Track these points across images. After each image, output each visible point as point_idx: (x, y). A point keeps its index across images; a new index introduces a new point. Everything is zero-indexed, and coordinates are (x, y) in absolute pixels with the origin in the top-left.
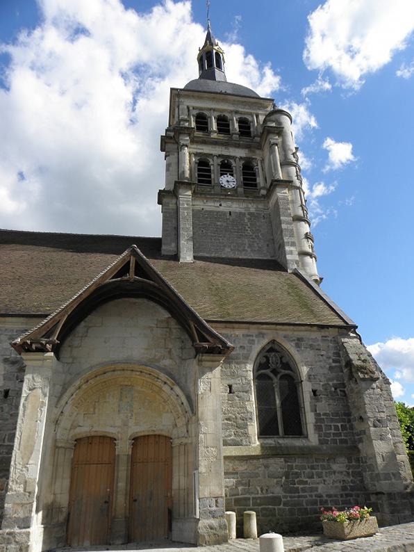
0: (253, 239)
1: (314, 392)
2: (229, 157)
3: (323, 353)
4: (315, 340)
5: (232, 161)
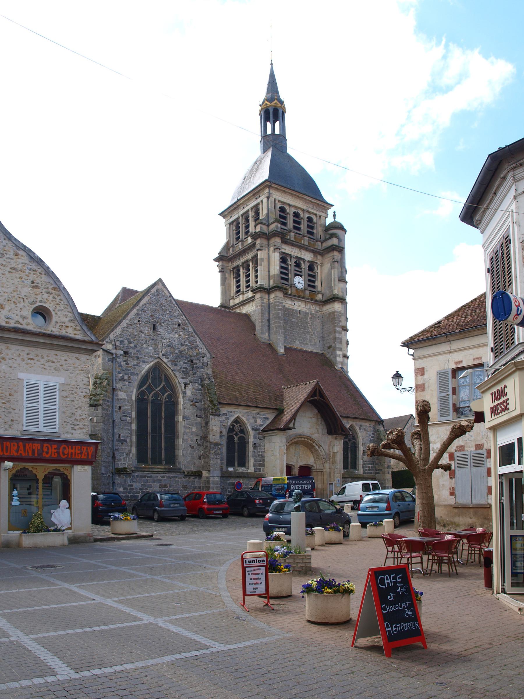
0: (312, 335)
1: (363, 450)
2: (301, 259)
3: (369, 433)
4: (366, 426)
5: (302, 262)
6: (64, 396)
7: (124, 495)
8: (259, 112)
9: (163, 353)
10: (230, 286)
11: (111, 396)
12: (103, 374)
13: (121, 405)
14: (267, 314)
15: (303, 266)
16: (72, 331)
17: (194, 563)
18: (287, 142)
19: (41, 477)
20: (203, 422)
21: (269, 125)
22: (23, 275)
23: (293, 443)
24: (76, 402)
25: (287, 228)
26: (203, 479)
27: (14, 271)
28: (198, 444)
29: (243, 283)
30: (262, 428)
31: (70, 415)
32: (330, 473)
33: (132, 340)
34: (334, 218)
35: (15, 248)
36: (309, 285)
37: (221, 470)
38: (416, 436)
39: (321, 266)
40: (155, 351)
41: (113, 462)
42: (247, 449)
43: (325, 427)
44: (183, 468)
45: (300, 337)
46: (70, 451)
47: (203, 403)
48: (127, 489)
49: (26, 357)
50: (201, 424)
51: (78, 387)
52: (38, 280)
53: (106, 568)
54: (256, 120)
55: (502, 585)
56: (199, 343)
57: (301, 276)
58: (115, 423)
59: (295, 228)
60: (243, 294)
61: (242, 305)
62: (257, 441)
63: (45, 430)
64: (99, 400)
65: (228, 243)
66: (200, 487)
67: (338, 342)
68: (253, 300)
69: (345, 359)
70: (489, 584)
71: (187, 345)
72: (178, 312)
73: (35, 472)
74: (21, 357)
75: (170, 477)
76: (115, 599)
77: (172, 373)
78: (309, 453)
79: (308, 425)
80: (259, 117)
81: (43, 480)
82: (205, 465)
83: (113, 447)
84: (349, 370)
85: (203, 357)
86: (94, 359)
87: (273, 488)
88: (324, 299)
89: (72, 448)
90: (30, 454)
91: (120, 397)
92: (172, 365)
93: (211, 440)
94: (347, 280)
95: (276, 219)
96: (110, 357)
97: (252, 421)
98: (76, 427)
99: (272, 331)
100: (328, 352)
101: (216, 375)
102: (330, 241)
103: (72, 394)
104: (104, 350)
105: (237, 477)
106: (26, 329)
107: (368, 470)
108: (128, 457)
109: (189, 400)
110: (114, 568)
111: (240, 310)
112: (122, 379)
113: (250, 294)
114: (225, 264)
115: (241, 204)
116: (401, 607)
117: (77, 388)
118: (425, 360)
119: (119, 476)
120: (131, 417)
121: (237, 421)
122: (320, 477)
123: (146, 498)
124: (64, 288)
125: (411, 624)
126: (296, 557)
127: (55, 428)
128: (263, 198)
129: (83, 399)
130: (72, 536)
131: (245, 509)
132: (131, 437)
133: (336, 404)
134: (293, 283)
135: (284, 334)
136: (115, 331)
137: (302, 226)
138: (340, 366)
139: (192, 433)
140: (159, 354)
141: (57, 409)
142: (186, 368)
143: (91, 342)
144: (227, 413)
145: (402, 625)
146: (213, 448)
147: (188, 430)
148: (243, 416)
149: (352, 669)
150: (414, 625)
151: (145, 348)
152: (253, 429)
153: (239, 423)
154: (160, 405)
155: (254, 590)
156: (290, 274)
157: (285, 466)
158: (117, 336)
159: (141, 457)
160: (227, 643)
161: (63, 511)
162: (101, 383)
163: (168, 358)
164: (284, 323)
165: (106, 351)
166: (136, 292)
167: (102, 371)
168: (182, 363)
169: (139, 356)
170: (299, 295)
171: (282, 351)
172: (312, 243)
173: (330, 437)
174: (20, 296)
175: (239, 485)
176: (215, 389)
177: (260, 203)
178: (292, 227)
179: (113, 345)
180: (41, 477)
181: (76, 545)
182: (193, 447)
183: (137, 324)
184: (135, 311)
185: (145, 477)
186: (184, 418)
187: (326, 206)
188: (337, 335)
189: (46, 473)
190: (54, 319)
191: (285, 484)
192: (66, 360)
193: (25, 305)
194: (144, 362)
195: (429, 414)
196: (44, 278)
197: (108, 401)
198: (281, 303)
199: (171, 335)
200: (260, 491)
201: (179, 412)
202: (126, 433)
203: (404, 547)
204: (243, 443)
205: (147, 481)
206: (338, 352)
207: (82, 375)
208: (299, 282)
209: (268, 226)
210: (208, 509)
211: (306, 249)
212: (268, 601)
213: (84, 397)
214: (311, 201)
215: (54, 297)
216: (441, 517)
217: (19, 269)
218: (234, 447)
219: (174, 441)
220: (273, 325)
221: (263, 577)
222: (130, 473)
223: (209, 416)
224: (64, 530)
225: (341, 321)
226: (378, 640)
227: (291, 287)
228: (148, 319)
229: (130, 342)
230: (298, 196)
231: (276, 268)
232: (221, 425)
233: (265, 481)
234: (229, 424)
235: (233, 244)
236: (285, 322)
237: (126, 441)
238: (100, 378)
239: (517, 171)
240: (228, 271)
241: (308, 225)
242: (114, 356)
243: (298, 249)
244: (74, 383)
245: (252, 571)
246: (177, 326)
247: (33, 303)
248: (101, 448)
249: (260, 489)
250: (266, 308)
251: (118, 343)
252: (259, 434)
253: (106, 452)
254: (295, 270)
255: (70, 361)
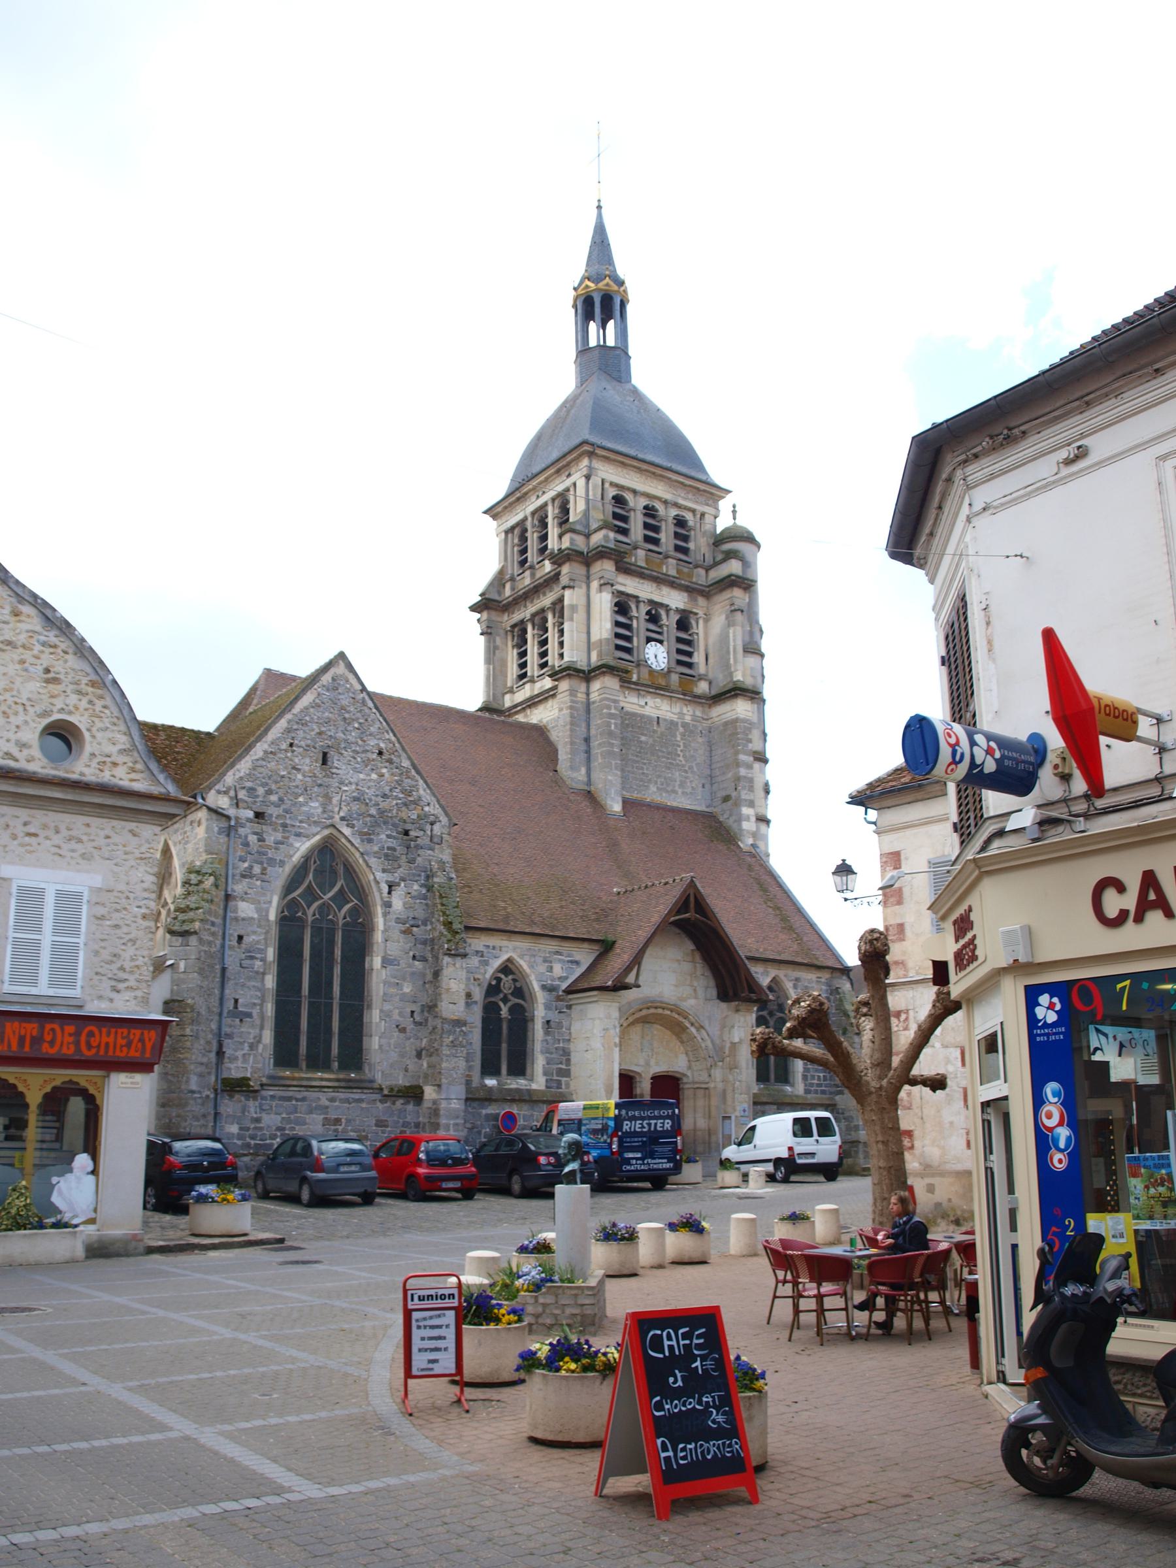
2: (661, 605)
4: (810, 981)
6: (99, 915)
7: (239, 1142)
8: (571, 302)
9: (342, 814)
10: (504, 663)
11: (221, 912)
12: (205, 863)
13: (241, 932)
14: (584, 725)
15: (664, 620)
16: (130, 773)
17: (345, 1305)
18: (632, 361)
19: (34, 1098)
20: (428, 971)
21: (593, 326)
22: (27, 656)
23: (632, 1024)
24: (125, 929)
25: (622, 541)
26: (426, 1104)
27: (9, 648)
28: (415, 1023)
29: (533, 657)
30: (564, 986)
31: (110, 958)
32: (724, 1091)
33: (273, 787)
34: (734, 518)
35: (13, 600)
36: (679, 662)
37: (468, 1083)
38: (865, 1010)
39: (707, 621)
40: (324, 812)
41: (217, 1064)
42: (530, 1034)
43: (712, 983)
44: (379, 1078)
45: (659, 776)
46: (105, 1039)
47: (429, 927)
48: (248, 1129)
49: (20, 830)
50: (424, 975)
51: (131, 895)
52: (58, 667)
53: (143, 1313)
54: (568, 318)
55: (997, 1363)
56: (423, 792)
57: (661, 642)
58: (228, 974)
59: (647, 539)
60: (532, 681)
61: (529, 706)
62: (554, 1016)
63: (51, 992)
64: (192, 921)
65: (501, 572)
66: (417, 1125)
67: (744, 788)
68: (554, 696)
69: (763, 826)
70: (975, 1362)
71: (397, 798)
72: (377, 725)
73: (21, 1088)
74: (9, 832)
75: (347, 1101)
76: (131, 1384)
77: (361, 861)
78: (675, 1043)
79: (670, 976)
80: (573, 311)
81: (40, 1106)
82: (430, 1071)
83: (220, 1028)
84: (770, 851)
85: (432, 824)
86: (188, 828)
87: (583, 1128)
88: (713, 693)
89: (109, 1033)
90: (15, 1047)
91: (242, 914)
92: (362, 841)
93: (445, 1014)
94: (763, 650)
95: (605, 521)
96: (224, 824)
97: (542, 968)
98: (121, 986)
99: (594, 764)
100: (724, 811)
101: (459, 863)
102: (722, 569)
103: (117, 911)
104: (210, 809)
105: (505, 1100)
106: (26, 771)
107: (818, 1085)
108: (253, 1051)
109: (398, 921)
110: (161, 1313)
111: (526, 716)
112: (247, 875)
113: (547, 683)
114: (495, 616)
115: (530, 491)
116: (700, 1402)
117: (128, 898)
118: (901, 834)
119: (231, 1097)
120: (263, 960)
121: (507, 969)
122: (700, 1103)
123: (287, 1148)
124: (115, 682)
125: (724, 1444)
126: (560, 1291)
127: (73, 987)
128: (578, 477)
129: (141, 921)
130: (95, 1238)
131: (516, 1178)
132: (261, 1005)
133: (719, 930)
134: (642, 657)
135: (623, 770)
136: (238, 767)
137: (663, 536)
138: (750, 841)
139: (403, 998)
140: (332, 818)
141: (82, 945)
142: (394, 849)
143: (165, 799)
144: (485, 951)
145: (701, 1446)
146: (450, 1032)
147: (393, 990)
148: (522, 956)
149: (569, 1544)
150: (730, 1445)
151: (302, 805)
152: (544, 987)
153: (512, 973)
154: (332, 932)
155: (431, 1366)
156: (635, 639)
157: (617, 1074)
158: (241, 778)
159: (285, 1055)
160: (332, 1482)
161: (79, 1179)
162: (200, 882)
163: (353, 826)
164: (623, 745)
165: (215, 812)
166: (293, 678)
167: (204, 857)
168: (383, 837)
169: (288, 822)
170: (656, 685)
171: (617, 807)
172: (686, 570)
173: (724, 1005)
174: (19, 701)
175: (510, 1118)
176: (457, 897)
177: (572, 489)
178: (640, 538)
179: (231, 798)
180: (34, 1098)
181: (102, 1261)
182: (403, 1030)
183: (286, 751)
184: (282, 723)
185: (289, 1099)
186: (386, 962)
187: (713, 493)
188: (743, 772)
189: (48, 1089)
190: (88, 749)
191: (608, 1118)
192: (108, 837)
193: (28, 718)
194: (298, 835)
195: (887, 957)
196: (73, 661)
197: (213, 924)
198: (615, 701)
199: (362, 776)
200: (553, 1136)
201: (375, 948)
202: (251, 996)
203: (803, 1268)
204: (521, 1020)
205: (296, 1107)
206: (746, 811)
207: (142, 869)
208: (657, 656)
209: (588, 536)
210: (428, 1178)
211: (672, 584)
212: (462, 1391)
213: (144, 917)
214: (682, 483)
215: (90, 702)
216: (950, 1200)
217: (19, 643)
218: (501, 1028)
219: (362, 1016)
220: (596, 751)
221: (450, 1334)
222: (256, 1091)
223: (441, 956)
224: (76, 1226)
225: (750, 741)
226: (639, 1482)
227: (638, 665)
228: (313, 740)
229: (269, 792)
230: (654, 473)
231: (603, 625)
232: (468, 979)
233: (566, 1110)
234: (488, 976)
235: (513, 575)
236: (625, 743)
237: (249, 1015)
238: (198, 872)
239: (970, 469)
240: (502, 632)
241: (676, 534)
242: (233, 823)
243: (654, 585)
244: (122, 887)
245: (425, 1319)
246: (375, 756)
247: (45, 714)
248: (192, 1030)
249: (555, 1132)
250: (582, 712)
251: (242, 795)
252: (558, 999)
253: (202, 1042)
254: (648, 630)
255: (116, 839)
